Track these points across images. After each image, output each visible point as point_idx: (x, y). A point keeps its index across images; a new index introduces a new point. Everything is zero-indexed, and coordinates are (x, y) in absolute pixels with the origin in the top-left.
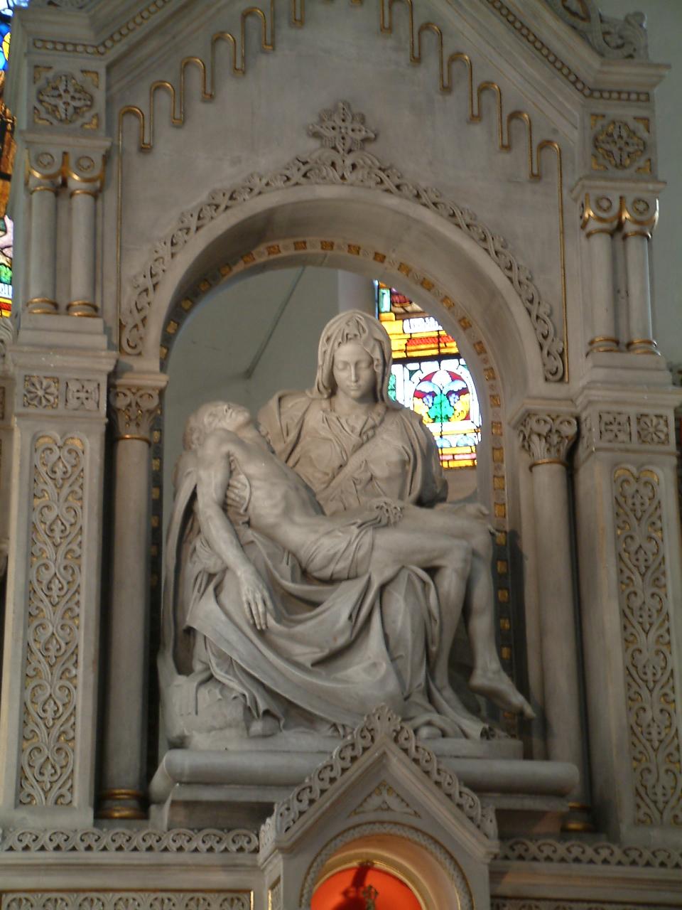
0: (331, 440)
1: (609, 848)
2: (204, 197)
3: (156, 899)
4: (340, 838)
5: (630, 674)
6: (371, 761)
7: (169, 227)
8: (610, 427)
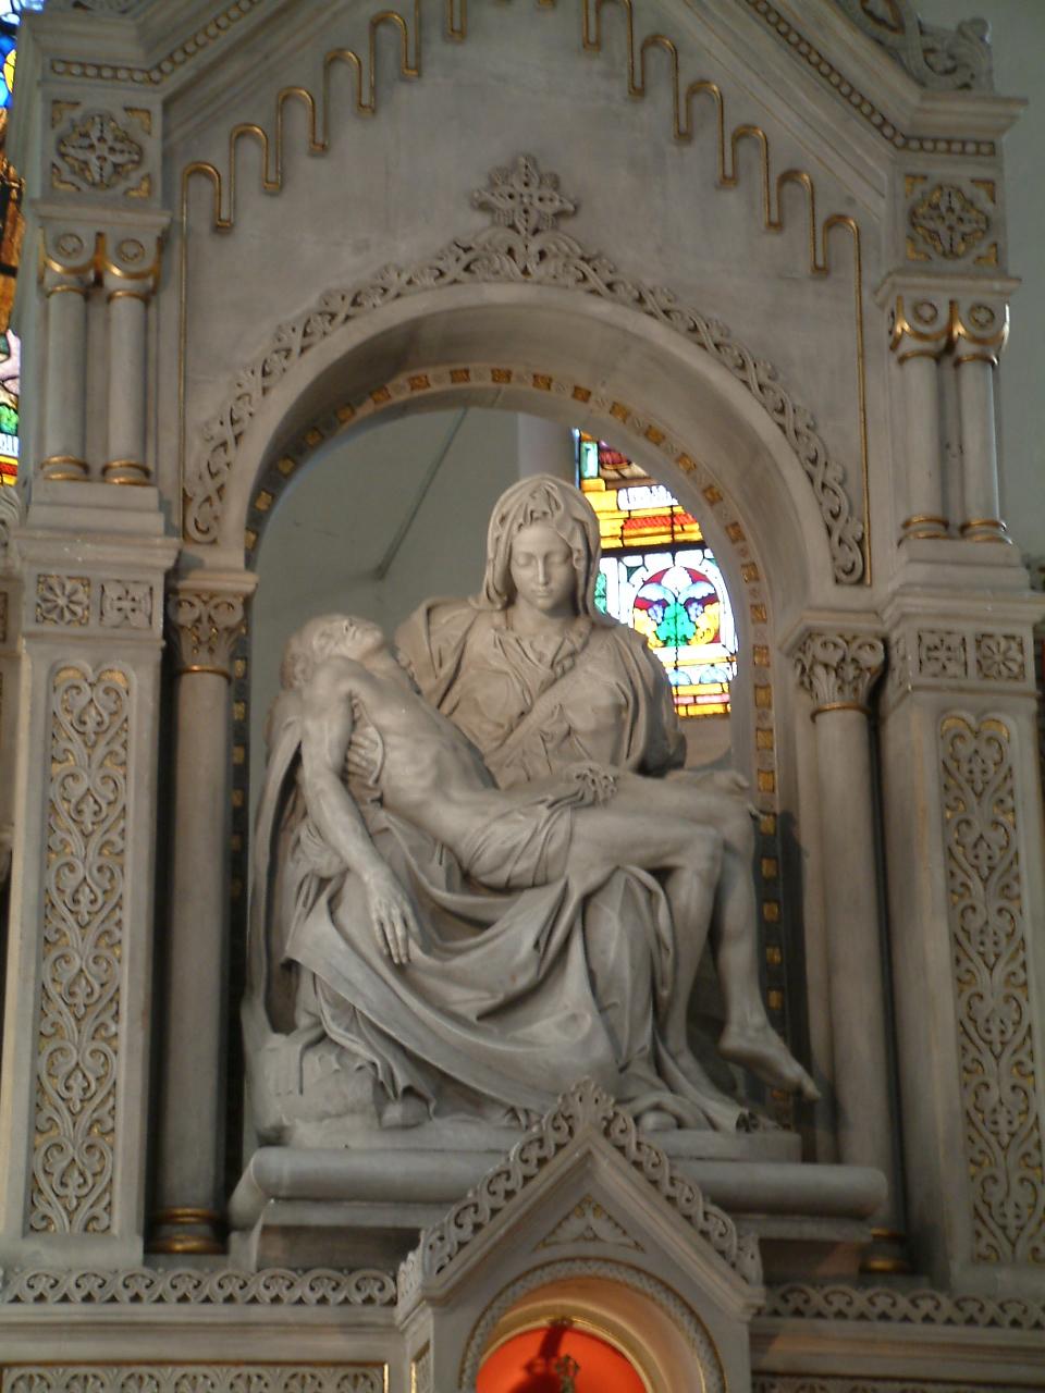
0: (506, 673)
1: (933, 1298)
2: (312, 301)
3: (239, 1376)
4: (521, 1282)
5: (966, 1032)
6: (568, 1164)
7: (258, 347)
8: (935, 654)
